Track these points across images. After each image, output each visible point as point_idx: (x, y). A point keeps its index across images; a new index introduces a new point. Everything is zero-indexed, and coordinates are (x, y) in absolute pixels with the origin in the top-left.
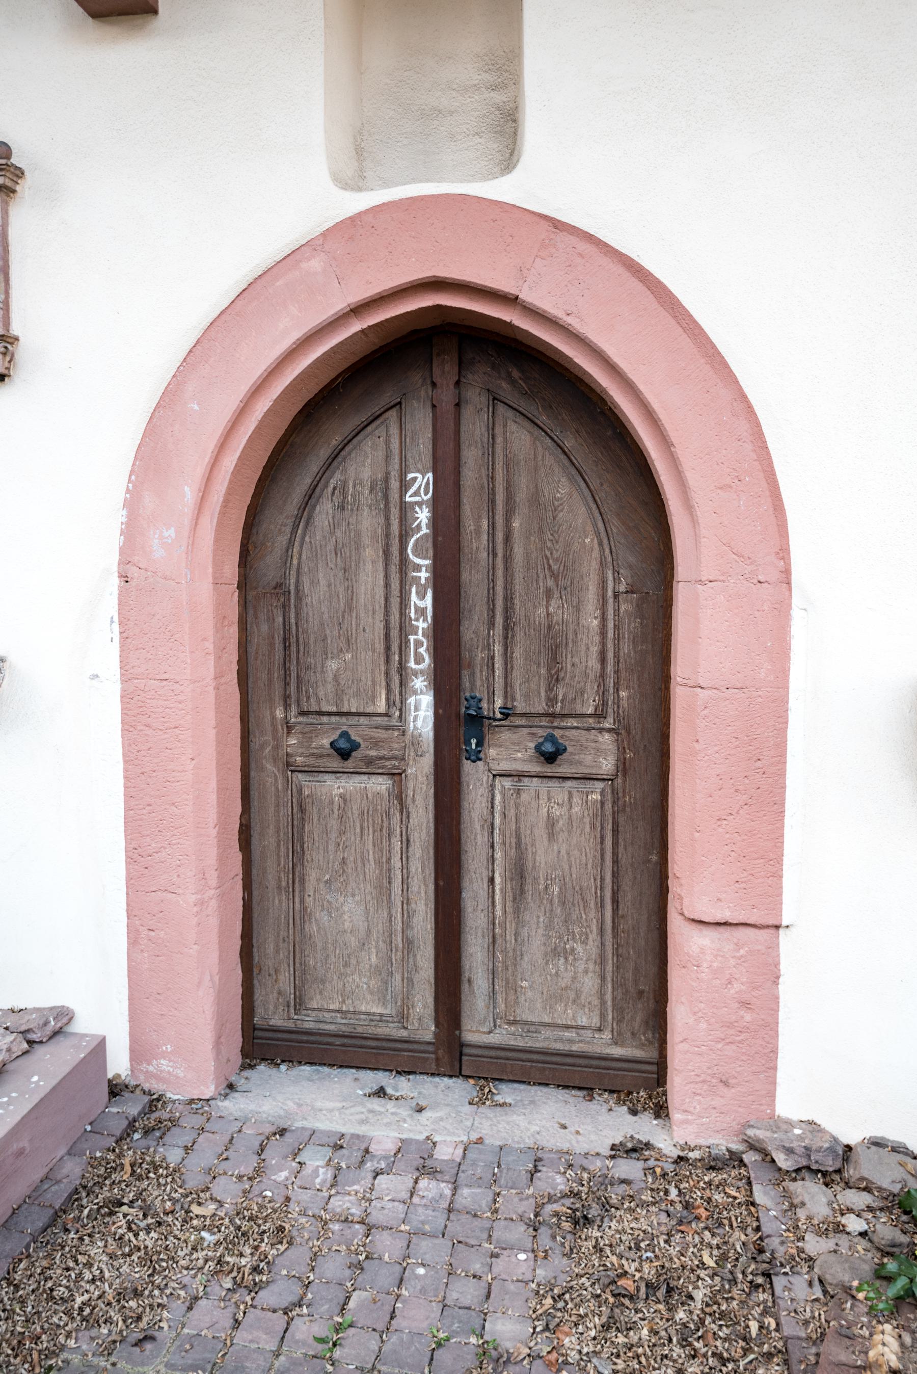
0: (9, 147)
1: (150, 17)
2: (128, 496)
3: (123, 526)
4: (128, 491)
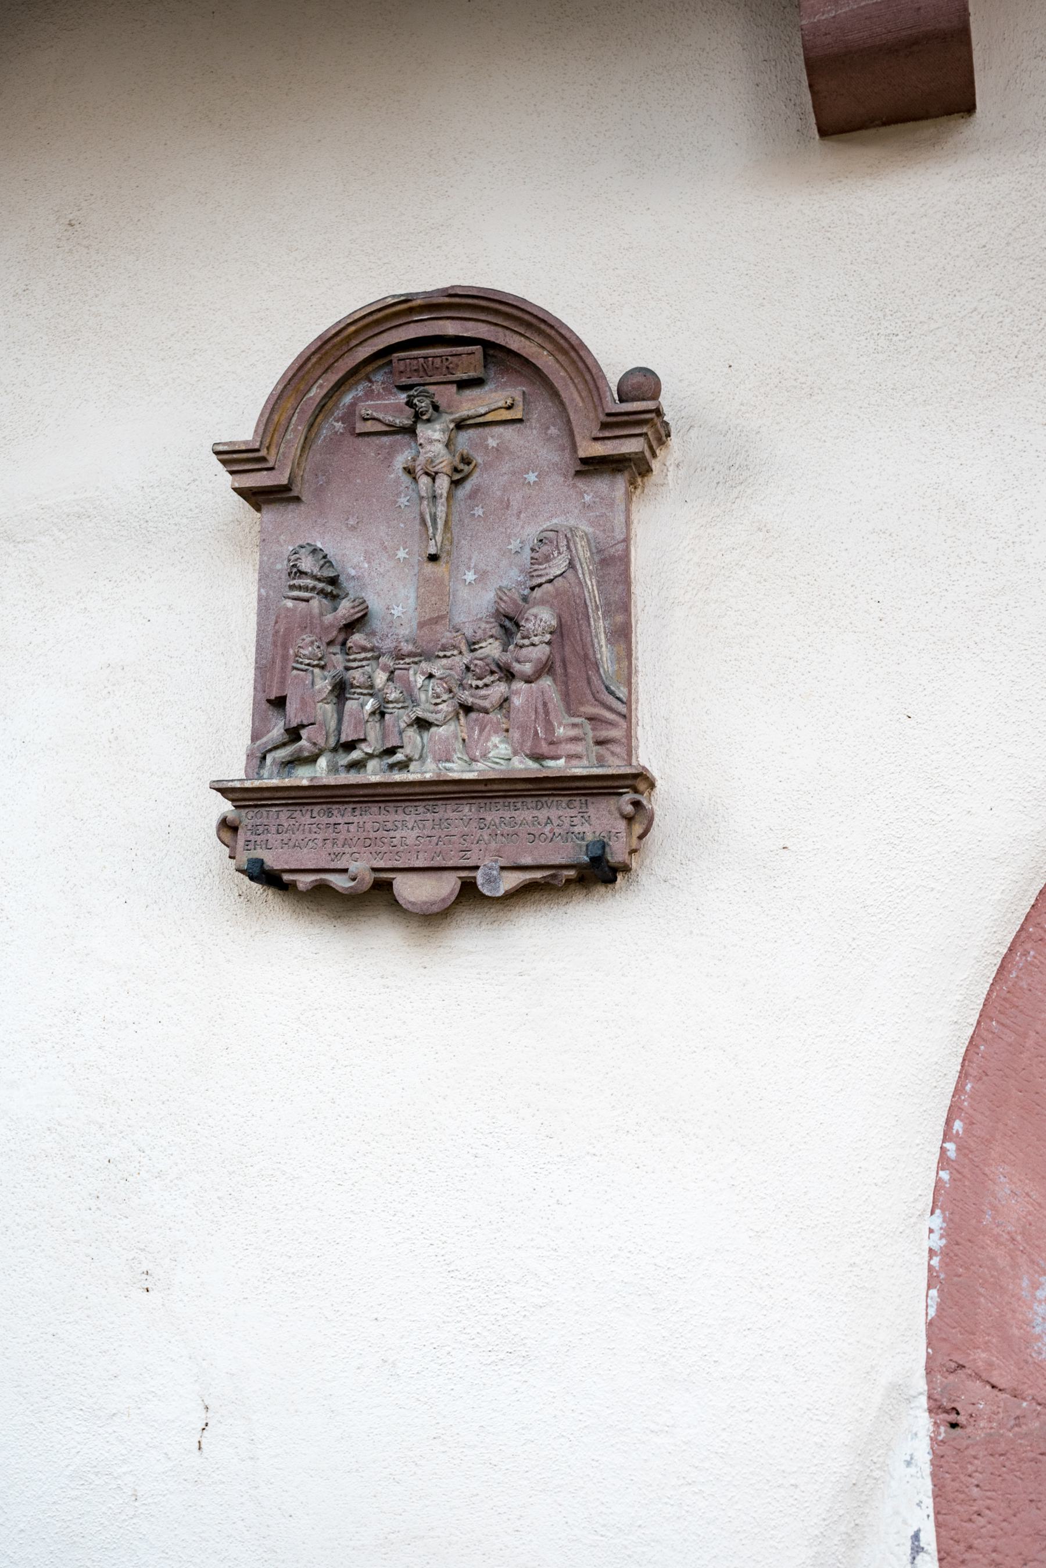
0: (653, 373)
1: (955, 121)
2: (945, 1175)
3: (935, 1261)
4: (944, 1161)
